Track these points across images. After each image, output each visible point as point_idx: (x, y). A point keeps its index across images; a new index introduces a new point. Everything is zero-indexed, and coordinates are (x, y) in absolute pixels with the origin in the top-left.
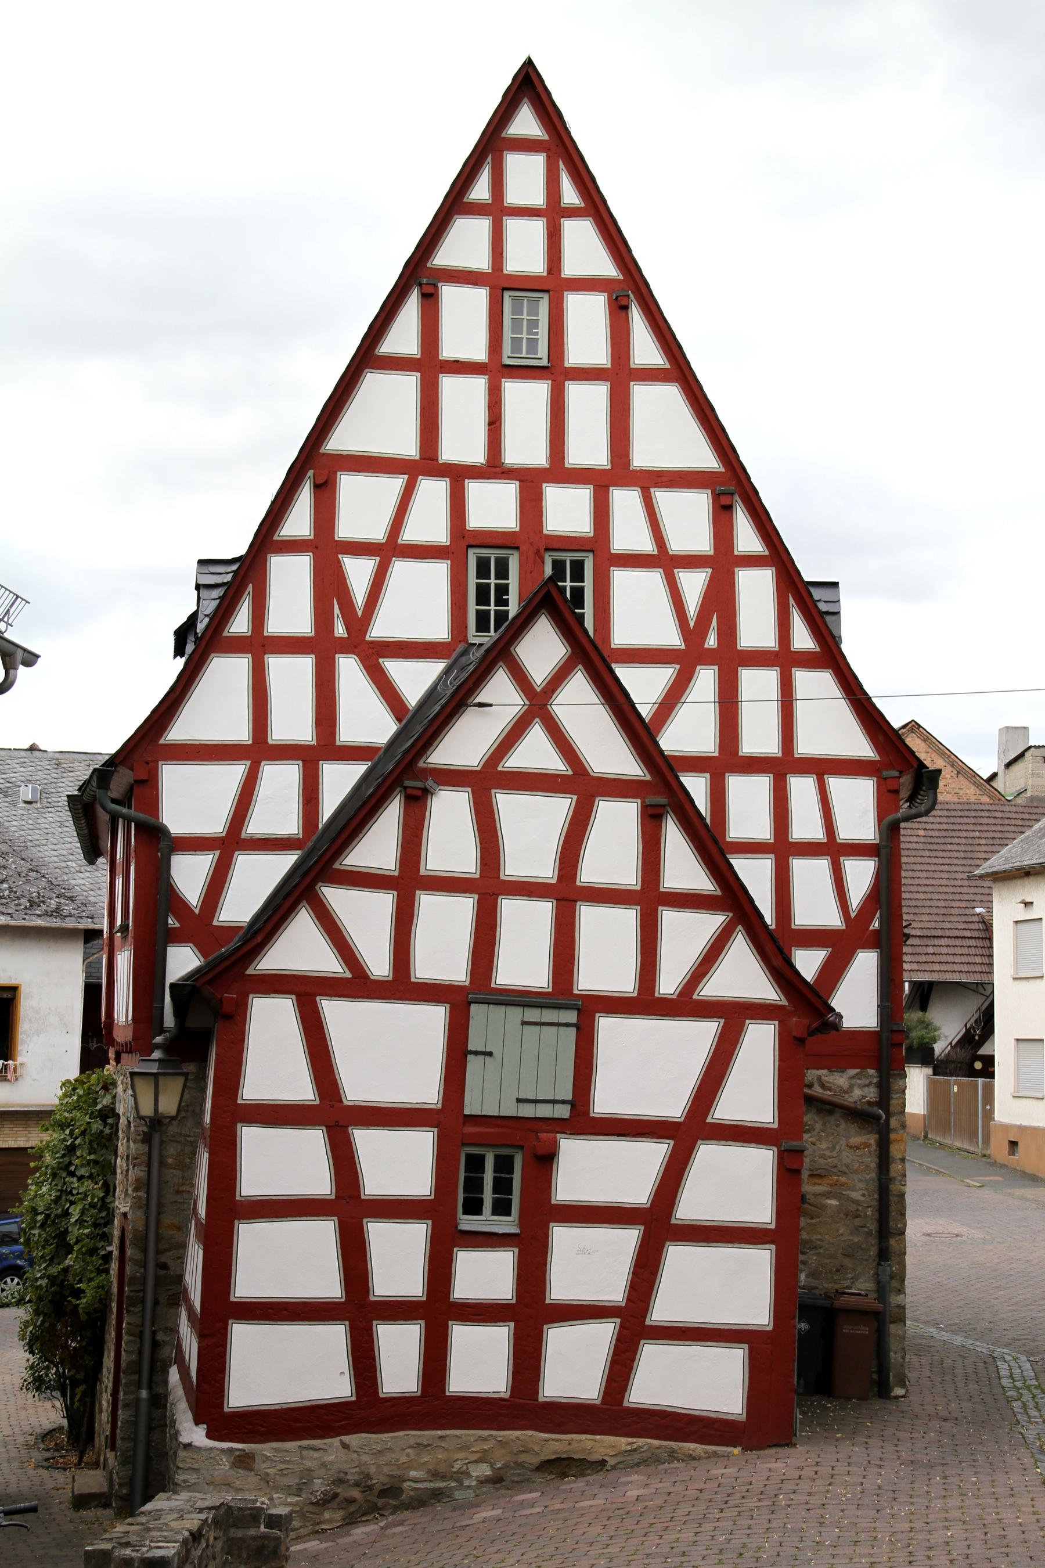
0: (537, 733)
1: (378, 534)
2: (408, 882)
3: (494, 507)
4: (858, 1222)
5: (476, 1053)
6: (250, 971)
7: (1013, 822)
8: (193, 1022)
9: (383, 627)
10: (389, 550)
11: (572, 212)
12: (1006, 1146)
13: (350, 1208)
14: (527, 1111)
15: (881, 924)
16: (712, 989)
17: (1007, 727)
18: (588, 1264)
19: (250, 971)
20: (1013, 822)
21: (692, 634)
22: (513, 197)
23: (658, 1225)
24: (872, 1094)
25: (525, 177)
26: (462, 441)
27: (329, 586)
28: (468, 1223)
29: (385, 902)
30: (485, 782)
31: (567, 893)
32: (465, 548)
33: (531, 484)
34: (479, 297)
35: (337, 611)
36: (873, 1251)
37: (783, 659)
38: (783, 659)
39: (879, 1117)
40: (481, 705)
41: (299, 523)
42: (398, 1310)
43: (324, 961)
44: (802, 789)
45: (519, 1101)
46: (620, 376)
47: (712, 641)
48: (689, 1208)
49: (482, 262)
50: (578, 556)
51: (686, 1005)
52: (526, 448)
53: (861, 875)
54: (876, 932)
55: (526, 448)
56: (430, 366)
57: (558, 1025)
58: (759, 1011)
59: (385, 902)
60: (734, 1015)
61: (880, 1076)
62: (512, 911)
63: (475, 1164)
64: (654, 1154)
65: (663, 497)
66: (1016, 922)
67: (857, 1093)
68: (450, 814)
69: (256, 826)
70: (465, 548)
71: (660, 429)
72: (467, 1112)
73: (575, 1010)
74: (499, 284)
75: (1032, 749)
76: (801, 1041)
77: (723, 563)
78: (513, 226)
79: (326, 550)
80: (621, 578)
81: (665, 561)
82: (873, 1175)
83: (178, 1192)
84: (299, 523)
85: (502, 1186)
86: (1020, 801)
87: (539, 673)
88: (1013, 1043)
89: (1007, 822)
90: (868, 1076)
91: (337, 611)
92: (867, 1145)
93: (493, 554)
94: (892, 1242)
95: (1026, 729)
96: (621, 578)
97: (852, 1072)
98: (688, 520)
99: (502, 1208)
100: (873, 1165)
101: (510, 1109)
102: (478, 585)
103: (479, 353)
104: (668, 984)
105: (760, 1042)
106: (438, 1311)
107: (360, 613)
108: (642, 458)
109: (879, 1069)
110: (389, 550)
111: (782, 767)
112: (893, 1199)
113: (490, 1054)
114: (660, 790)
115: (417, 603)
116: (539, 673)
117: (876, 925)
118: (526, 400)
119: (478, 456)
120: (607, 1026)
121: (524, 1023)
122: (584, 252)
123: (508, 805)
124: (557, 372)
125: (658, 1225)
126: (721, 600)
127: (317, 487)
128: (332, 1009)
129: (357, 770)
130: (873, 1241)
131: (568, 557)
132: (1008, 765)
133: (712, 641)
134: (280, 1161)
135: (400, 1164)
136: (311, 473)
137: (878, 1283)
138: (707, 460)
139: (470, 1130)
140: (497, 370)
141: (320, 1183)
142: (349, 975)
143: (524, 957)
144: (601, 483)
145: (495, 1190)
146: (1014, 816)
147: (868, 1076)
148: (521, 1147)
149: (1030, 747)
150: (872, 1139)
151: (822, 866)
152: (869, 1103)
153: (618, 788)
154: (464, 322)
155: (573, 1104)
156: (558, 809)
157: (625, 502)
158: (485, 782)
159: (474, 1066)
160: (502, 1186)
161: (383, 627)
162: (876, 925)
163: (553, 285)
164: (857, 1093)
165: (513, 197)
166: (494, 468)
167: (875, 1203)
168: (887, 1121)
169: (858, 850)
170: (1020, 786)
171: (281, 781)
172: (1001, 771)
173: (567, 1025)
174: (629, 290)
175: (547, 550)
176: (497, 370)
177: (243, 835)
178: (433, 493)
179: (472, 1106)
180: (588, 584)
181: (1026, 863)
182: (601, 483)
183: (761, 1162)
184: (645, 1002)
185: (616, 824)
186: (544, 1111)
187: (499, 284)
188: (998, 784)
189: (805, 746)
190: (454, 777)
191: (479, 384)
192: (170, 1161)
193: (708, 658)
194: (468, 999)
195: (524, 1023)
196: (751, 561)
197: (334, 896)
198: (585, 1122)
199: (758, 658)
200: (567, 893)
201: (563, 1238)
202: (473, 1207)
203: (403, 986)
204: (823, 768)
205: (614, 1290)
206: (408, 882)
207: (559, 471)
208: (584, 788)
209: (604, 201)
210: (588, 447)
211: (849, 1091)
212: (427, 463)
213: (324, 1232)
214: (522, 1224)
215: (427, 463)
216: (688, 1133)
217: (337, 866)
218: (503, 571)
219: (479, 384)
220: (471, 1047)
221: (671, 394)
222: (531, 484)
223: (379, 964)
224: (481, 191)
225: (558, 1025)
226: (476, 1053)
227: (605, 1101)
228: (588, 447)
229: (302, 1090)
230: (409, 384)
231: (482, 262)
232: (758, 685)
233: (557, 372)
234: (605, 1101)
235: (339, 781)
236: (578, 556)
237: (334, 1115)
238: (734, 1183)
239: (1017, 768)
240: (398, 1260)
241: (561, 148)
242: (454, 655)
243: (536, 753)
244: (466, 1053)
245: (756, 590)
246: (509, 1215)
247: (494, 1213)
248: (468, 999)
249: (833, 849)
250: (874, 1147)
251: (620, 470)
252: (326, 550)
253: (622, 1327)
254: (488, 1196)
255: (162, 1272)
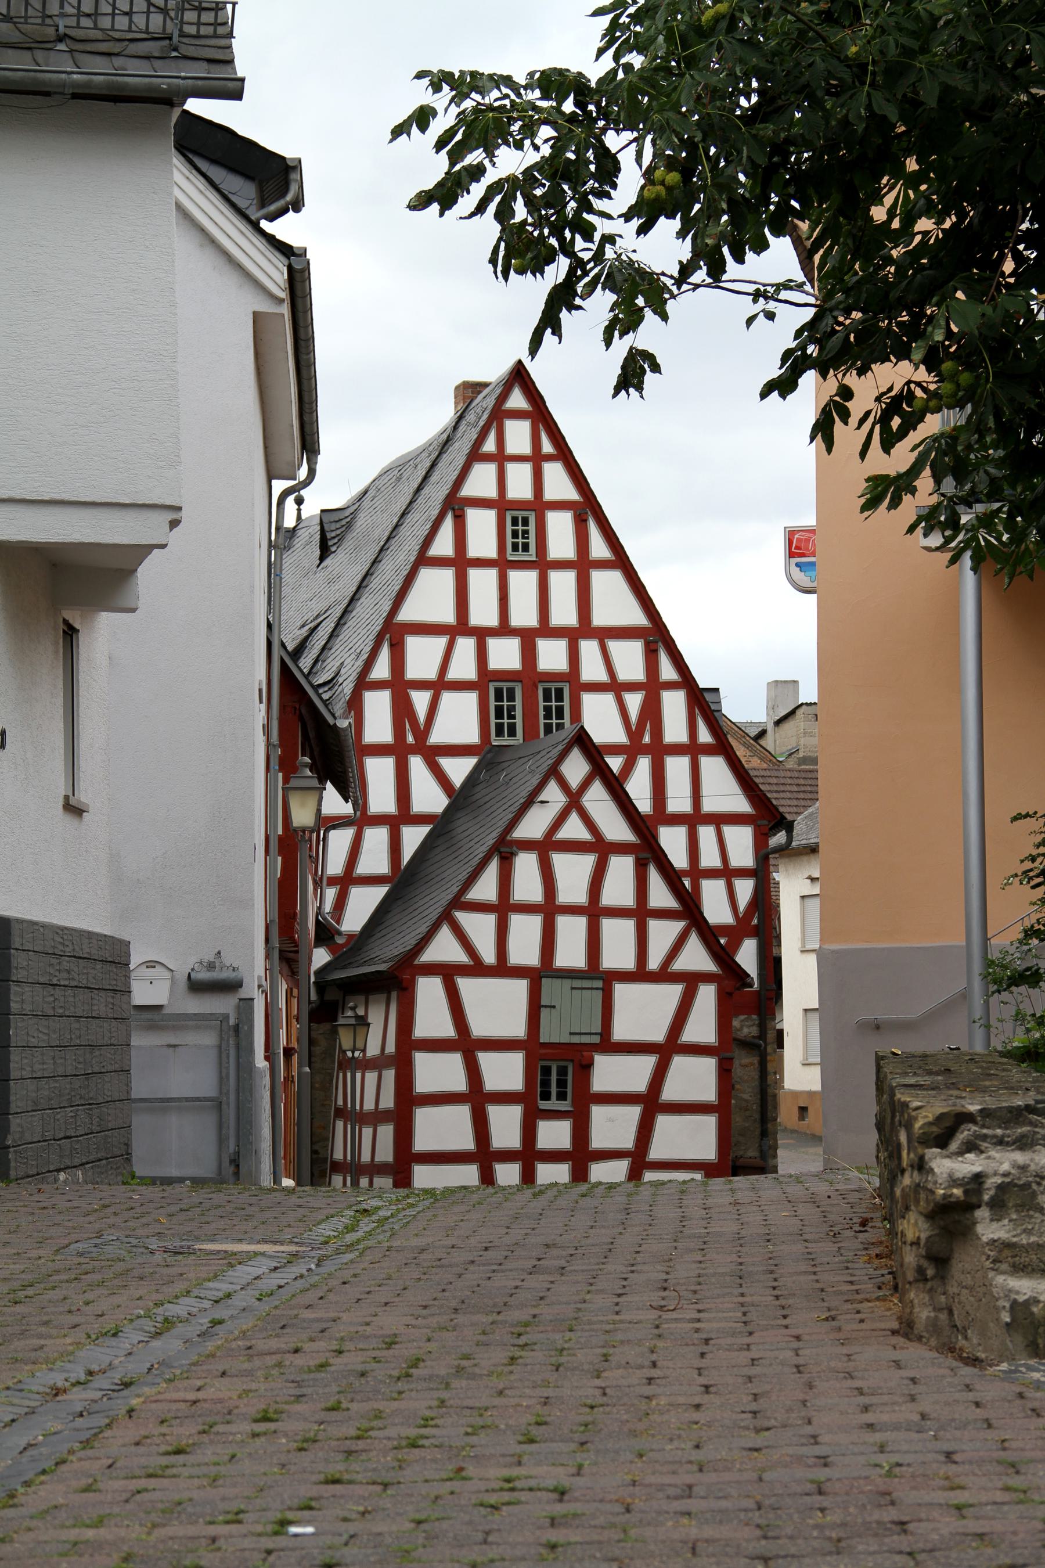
0: (574, 819)
1: (432, 674)
2: (504, 908)
3: (505, 654)
4: (748, 1113)
5: (546, 1006)
6: (416, 962)
7: (788, 788)
8: (329, 997)
9: (437, 737)
10: (440, 685)
11: (549, 458)
12: (796, 1112)
13: (477, 1098)
14: (576, 1039)
15: (759, 920)
16: (681, 964)
17: (777, 681)
18: (613, 1127)
19: (416, 962)
20: (788, 788)
21: (634, 734)
22: (511, 449)
23: (651, 1104)
24: (755, 1031)
25: (518, 436)
26: (483, 612)
27: (402, 710)
28: (543, 1105)
29: (490, 920)
30: (546, 847)
31: (594, 911)
32: (486, 681)
33: (528, 638)
34: (490, 516)
35: (408, 726)
36: (758, 1132)
37: (692, 750)
38: (692, 750)
39: (760, 1046)
40: (542, 802)
41: (381, 670)
42: (507, 1156)
43: (457, 955)
44: (706, 834)
45: (571, 1034)
46: (583, 566)
47: (647, 739)
48: (670, 1093)
49: (492, 493)
50: (559, 685)
51: (664, 975)
52: (523, 614)
53: (745, 889)
54: (756, 926)
55: (523, 614)
56: (461, 563)
57: (592, 989)
58: (705, 977)
59: (490, 920)
60: (692, 981)
61: (760, 1020)
62: (563, 922)
63: (546, 1071)
64: (648, 1063)
65: (613, 645)
66: (803, 897)
67: (746, 1030)
68: (526, 865)
69: (363, 868)
70: (486, 681)
71: (612, 601)
72: (541, 1041)
73: (599, 979)
74: (501, 504)
75: (804, 707)
76: (730, 994)
77: (652, 688)
78: (511, 468)
79: (400, 687)
80: (588, 700)
81: (615, 687)
82: (757, 1083)
83: (323, 1105)
84: (381, 670)
85: (562, 1083)
86: (791, 764)
87: (574, 782)
88: (801, 1013)
89: (782, 788)
90: (753, 1020)
91: (408, 726)
92: (752, 1064)
93: (505, 685)
94: (769, 1126)
95: (795, 682)
96: (588, 700)
97: (742, 1017)
98: (630, 660)
99: (562, 1096)
100: (757, 1077)
101: (566, 1039)
102: (496, 706)
103: (492, 553)
104: (654, 963)
105: (707, 996)
106: (529, 1155)
107: (422, 728)
108: (600, 618)
109: (759, 1015)
110: (440, 685)
111: (694, 820)
112: (770, 1099)
113: (554, 1007)
114: (647, 853)
115: (458, 720)
116: (574, 782)
117: (755, 921)
118: (523, 583)
119: (492, 620)
120: (621, 990)
121: (572, 988)
122: (558, 484)
123: (560, 861)
124: (544, 565)
125: (651, 1104)
126: (652, 711)
127: (392, 646)
128: (464, 984)
129: (424, 830)
130: (758, 1125)
131: (553, 686)
132: (778, 723)
133: (647, 739)
134: (440, 1072)
135: (504, 1072)
136: (388, 636)
137: (761, 1151)
138: (638, 618)
139: (543, 1051)
140: (502, 565)
141: (459, 1083)
142: (472, 963)
143: (571, 952)
144: (573, 636)
145: (558, 1087)
146: (789, 781)
147: (753, 1020)
148: (572, 1061)
149: (802, 704)
150: (756, 1060)
151: (720, 884)
152: (753, 1037)
153: (621, 848)
154: (483, 533)
155: (601, 1034)
156: (587, 862)
157: (589, 649)
158: (546, 847)
159: (544, 1013)
160: (562, 1083)
161: (437, 737)
162: (755, 921)
163: (539, 505)
164: (746, 1030)
165: (511, 449)
166: (504, 629)
167: (758, 1101)
168: (765, 1048)
169: (743, 873)
170: (791, 744)
171: (376, 838)
172: (770, 727)
173: (597, 989)
174: (587, 508)
175: (540, 682)
176: (502, 565)
177: (354, 875)
178: (466, 646)
179: (546, 1036)
180: (566, 703)
181: (812, 841)
182: (573, 636)
183: (708, 1065)
184: (641, 974)
185: (621, 871)
186: (585, 1039)
187: (501, 504)
188: (768, 742)
189: (709, 806)
190: (527, 845)
191: (492, 573)
192: (317, 1085)
193: (644, 750)
194: (540, 976)
195: (572, 988)
196: (671, 686)
197: (463, 918)
198: (610, 1046)
199: (677, 749)
200: (594, 911)
201: (598, 1113)
202: (546, 1096)
203: (502, 969)
204: (719, 820)
205: (627, 1141)
206: (504, 908)
207: (546, 629)
208: (601, 848)
209: (571, 452)
210: (564, 614)
211: (741, 1029)
212: (461, 627)
213: (463, 1113)
214: (574, 1103)
215: (461, 627)
216: (667, 1050)
217: (463, 899)
218: (511, 697)
219: (492, 573)
220: (543, 1003)
221: (615, 577)
222: (528, 638)
223: (489, 956)
224: (490, 446)
225: (592, 989)
226: (546, 1006)
227: (621, 1032)
228: (564, 614)
229: (447, 1030)
230: (448, 575)
231: (492, 493)
232: (677, 768)
233: (544, 565)
234: (621, 1032)
235: (413, 837)
236: (559, 685)
237: (466, 1045)
238: (694, 1078)
239: (788, 726)
240: (506, 1126)
241: (540, 415)
242: (483, 753)
243: (574, 829)
244: (540, 1007)
245: (674, 706)
246: (566, 1100)
247: (558, 1099)
248: (540, 976)
249: (727, 873)
250: (757, 1065)
251: (585, 628)
252: (400, 687)
253: (633, 1162)
254: (554, 1090)
255: (315, 1156)
